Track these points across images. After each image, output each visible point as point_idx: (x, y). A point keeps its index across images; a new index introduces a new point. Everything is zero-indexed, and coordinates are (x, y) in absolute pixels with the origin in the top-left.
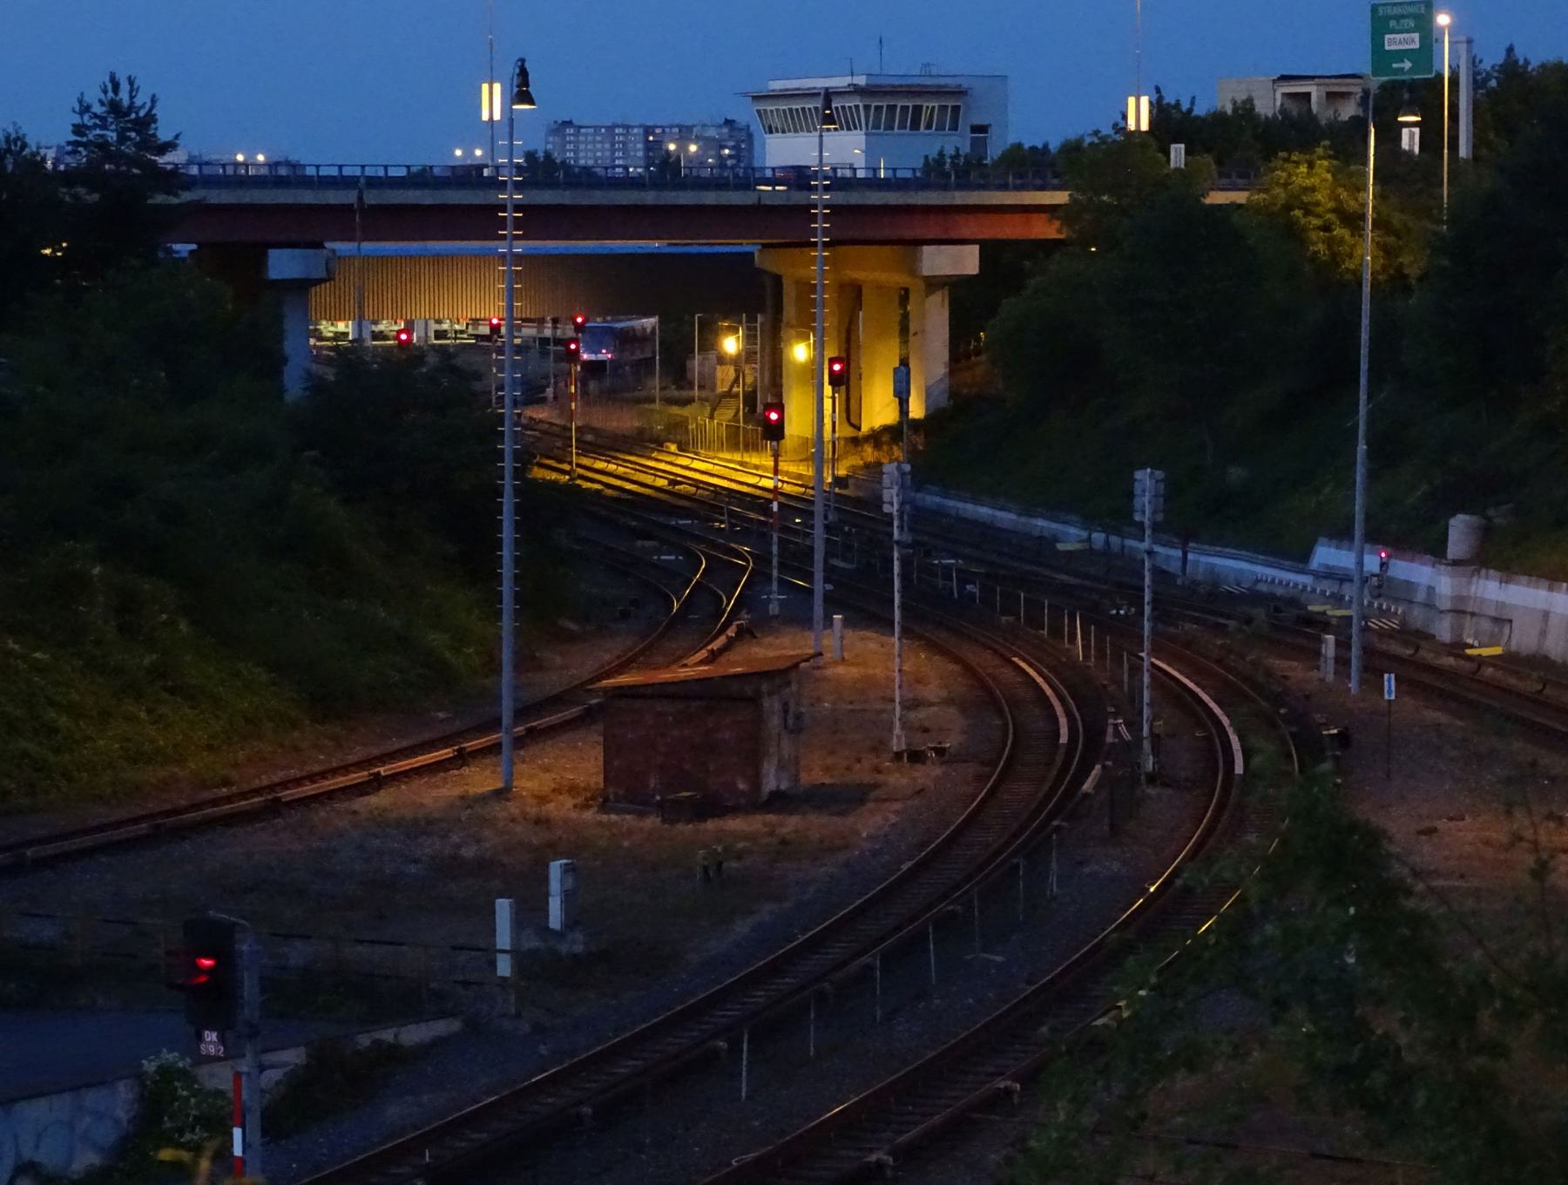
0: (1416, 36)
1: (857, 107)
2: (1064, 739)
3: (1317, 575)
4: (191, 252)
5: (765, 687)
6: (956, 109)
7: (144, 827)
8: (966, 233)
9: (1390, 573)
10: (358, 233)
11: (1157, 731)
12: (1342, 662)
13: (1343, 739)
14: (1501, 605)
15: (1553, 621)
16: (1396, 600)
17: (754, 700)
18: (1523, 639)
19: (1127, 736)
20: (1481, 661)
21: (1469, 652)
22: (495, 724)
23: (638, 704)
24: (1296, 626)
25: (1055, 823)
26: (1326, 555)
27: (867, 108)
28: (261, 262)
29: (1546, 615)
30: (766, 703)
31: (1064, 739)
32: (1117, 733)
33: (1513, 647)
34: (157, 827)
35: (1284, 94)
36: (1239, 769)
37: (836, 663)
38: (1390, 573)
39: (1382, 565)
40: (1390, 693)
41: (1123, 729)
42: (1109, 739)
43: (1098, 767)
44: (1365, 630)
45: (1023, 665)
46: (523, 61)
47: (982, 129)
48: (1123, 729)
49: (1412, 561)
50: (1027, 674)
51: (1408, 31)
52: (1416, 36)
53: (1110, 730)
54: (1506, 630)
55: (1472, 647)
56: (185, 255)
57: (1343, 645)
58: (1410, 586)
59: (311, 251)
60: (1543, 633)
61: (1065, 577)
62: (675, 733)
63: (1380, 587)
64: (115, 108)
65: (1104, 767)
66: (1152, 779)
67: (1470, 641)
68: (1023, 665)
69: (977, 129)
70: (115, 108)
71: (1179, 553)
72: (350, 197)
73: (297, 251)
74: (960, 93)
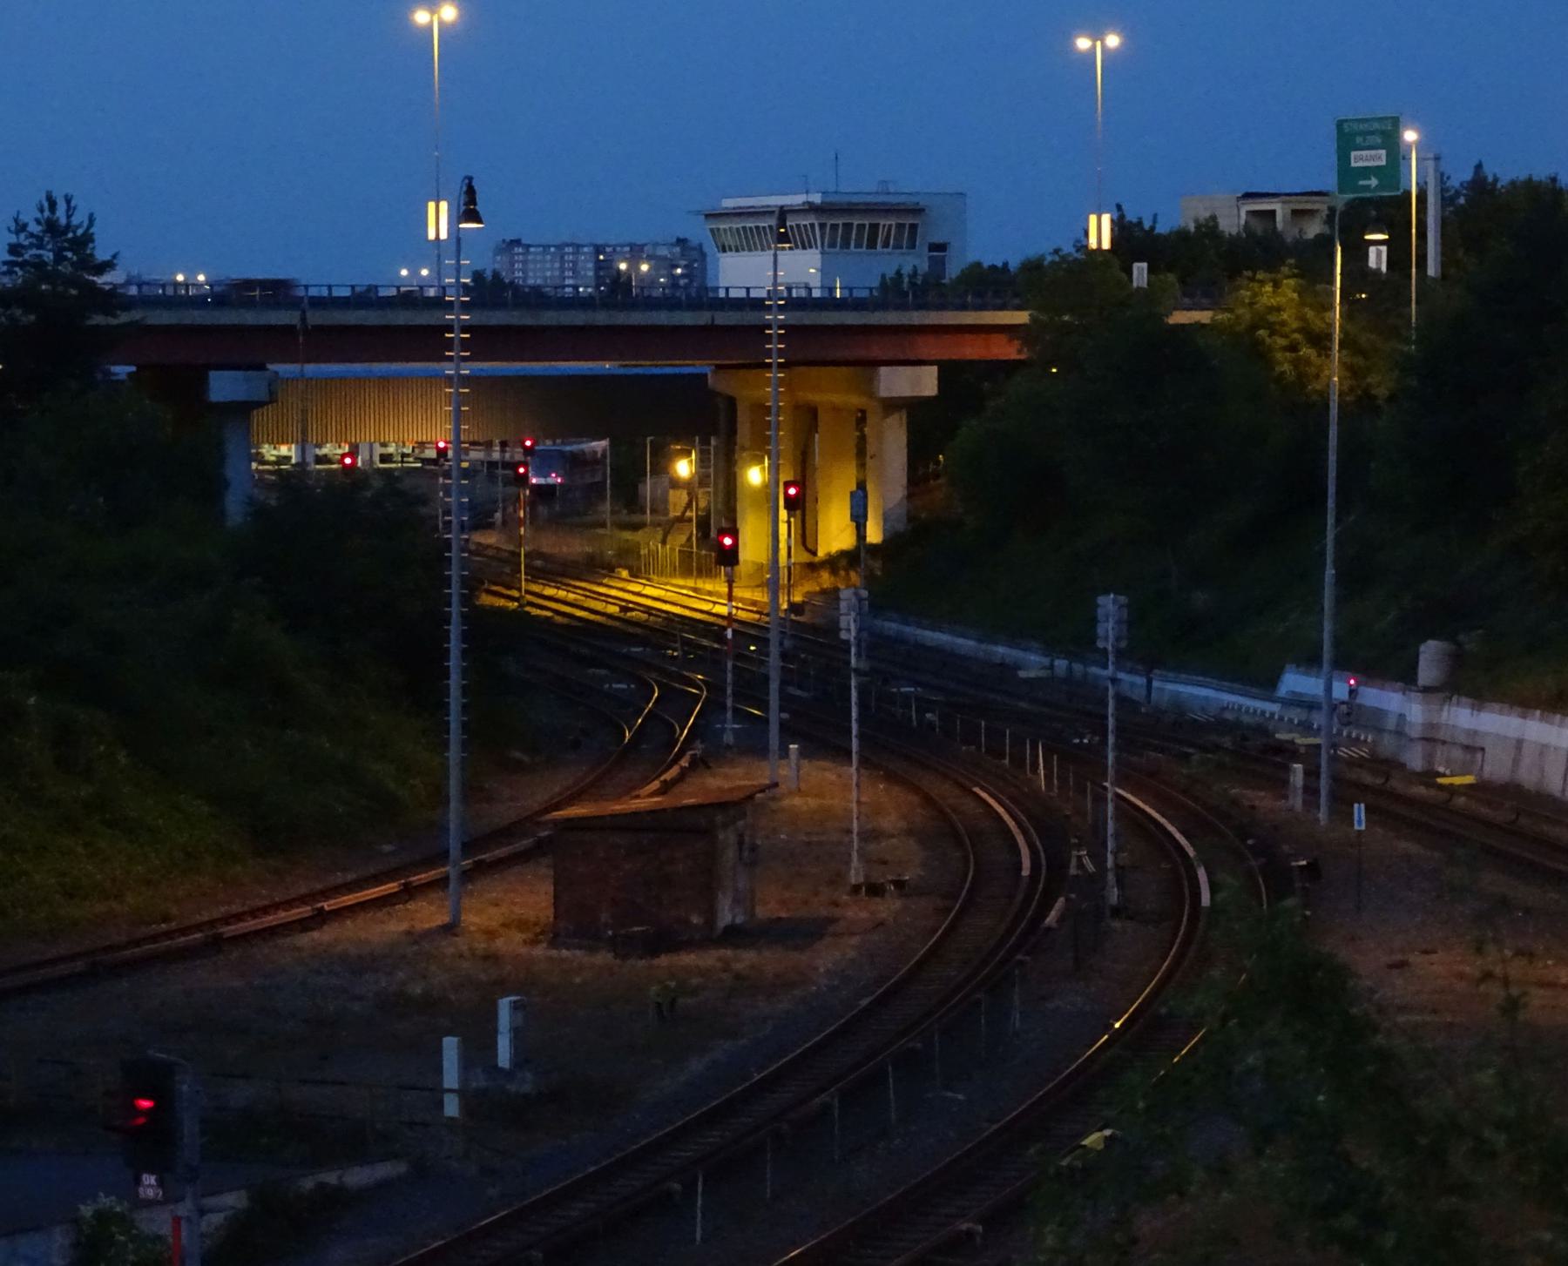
0: (1383, 152)
1: (812, 225)
2: (1025, 873)
4: (129, 374)
6: (913, 227)
8: (924, 353)
12: (1311, 791)
13: (1313, 870)
14: (1474, 733)
15: (1526, 750)
18: (1496, 767)
21: (1440, 780)
22: (443, 857)
26: (1295, 682)
27: (822, 226)
31: (1025, 873)
32: (1081, 866)
35: (1250, 213)
36: (1206, 900)
41: (1087, 861)
42: (1073, 871)
43: (1061, 900)
44: (1334, 759)
45: (984, 795)
47: (941, 247)
48: (1087, 861)
52: (1383, 152)
53: (1074, 862)
55: (1444, 775)
57: (1312, 773)
58: (1379, 714)
60: (1516, 762)
62: (627, 867)
64: (51, 227)
66: (1116, 912)
68: (984, 795)
70: (51, 227)
74: (917, 211)
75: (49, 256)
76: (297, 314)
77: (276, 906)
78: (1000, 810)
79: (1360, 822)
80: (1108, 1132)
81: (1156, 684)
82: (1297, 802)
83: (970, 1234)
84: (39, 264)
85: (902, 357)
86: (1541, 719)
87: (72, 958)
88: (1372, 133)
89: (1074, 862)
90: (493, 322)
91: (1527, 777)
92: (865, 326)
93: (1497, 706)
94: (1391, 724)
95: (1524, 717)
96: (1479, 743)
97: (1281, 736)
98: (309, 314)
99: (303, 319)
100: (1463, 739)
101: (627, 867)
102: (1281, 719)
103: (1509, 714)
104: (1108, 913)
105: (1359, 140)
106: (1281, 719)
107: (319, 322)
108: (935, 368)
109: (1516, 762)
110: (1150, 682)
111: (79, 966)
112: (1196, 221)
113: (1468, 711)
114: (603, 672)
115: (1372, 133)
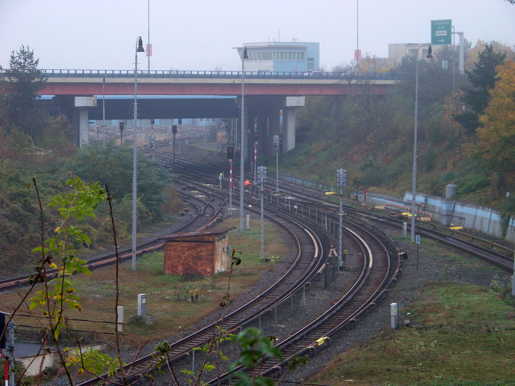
0: (446, 31)
1: (271, 52)
2: (316, 256)
3: (405, 204)
4: (53, 98)
5: (216, 238)
6: (303, 53)
7: (13, 283)
8: (301, 93)
9: (428, 203)
10: (136, 92)
11: (344, 253)
12: (409, 231)
13: (405, 256)
14: (462, 213)
15: (477, 218)
16: (430, 211)
17: (212, 243)
18: (468, 224)
19: (336, 255)
20: (453, 231)
21: (451, 228)
22: (130, 251)
23: (175, 244)
24: (396, 220)
25: (307, 283)
26: (408, 197)
27: (274, 52)
28: (284, 101)
29: (475, 216)
30: (217, 244)
31: (316, 256)
32: (333, 254)
33: (465, 226)
34: (18, 282)
35: (409, 50)
36: (371, 265)
37: (270, 232)
38: (428, 203)
39: (425, 200)
40: (418, 241)
41: (335, 253)
42: (330, 256)
43: (324, 265)
44: (416, 221)
45: (307, 231)
46: (141, 37)
47: (312, 59)
48: (335, 253)
49: (434, 199)
50: (307, 234)
51: (442, 30)
52: (446, 31)
53: (331, 253)
54: (463, 221)
55: (452, 226)
56: (51, 99)
57: (409, 225)
58: (434, 207)
59: (89, 98)
60: (474, 222)
61: (326, 204)
62: (187, 253)
63: (425, 207)
64: (23, 52)
65: (326, 265)
66: (341, 269)
67: (452, 225)
68: (307, 231)
69: (309, 59)
70: (23, 52)
71: (363, 196)
72: (100, 80)
73: (85, 98)
74: (304, 48)
75: (22, 61)
76: (102, 79)
77: (99, 260)
78: (312, 236)
79: (418, 241)
80: (326, 338)
81: (367, 197)
82: (405, 233)
83: (277, 369)
84: (20, 64)
85: (294, 94)
86: (482, 209)
87: (26, 278)
88: (443, 25)
89: (331, 253)
90: (172, 82)
91: (477, 227)
92: (282, 84)
93: (469, 205)
94: (437, 210)
95: (477, 208)
96: (463, 216)
97: (404, 214)
98: (106, 79)
99: (104, 80)
100: (459, 216)
101: (187, 253)
102: (404, 209)
103: (472, 208)
104: (338, 268)
105: (438, 27)
106: (404, 209)
107: (109, 82)
108: (304, 97)
109: (474, 222)
110: (365, 196)
111: (13, 283)
112: (479, 42)
113: (460, 206)
114: (197, 192)
115: (443, 25)
